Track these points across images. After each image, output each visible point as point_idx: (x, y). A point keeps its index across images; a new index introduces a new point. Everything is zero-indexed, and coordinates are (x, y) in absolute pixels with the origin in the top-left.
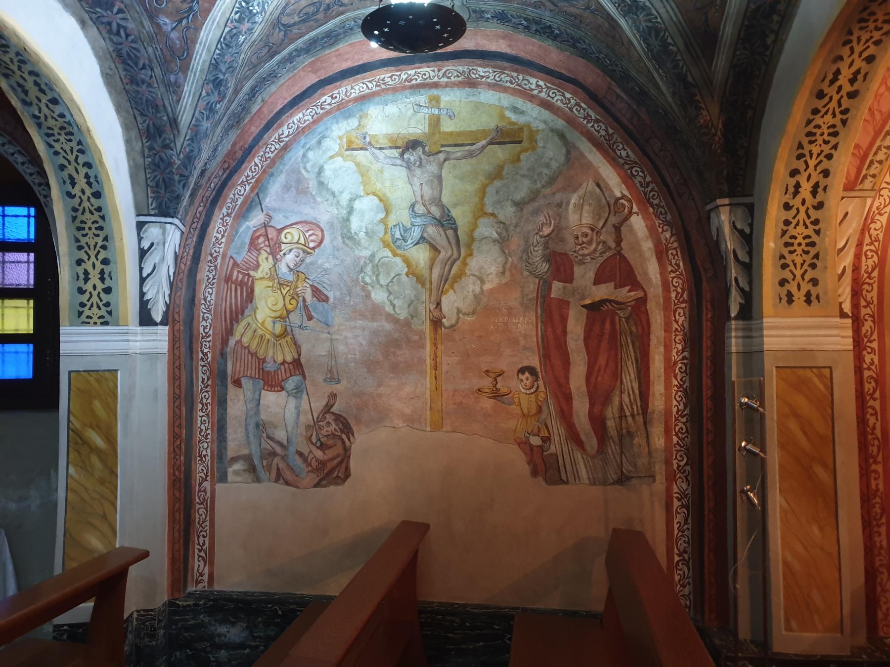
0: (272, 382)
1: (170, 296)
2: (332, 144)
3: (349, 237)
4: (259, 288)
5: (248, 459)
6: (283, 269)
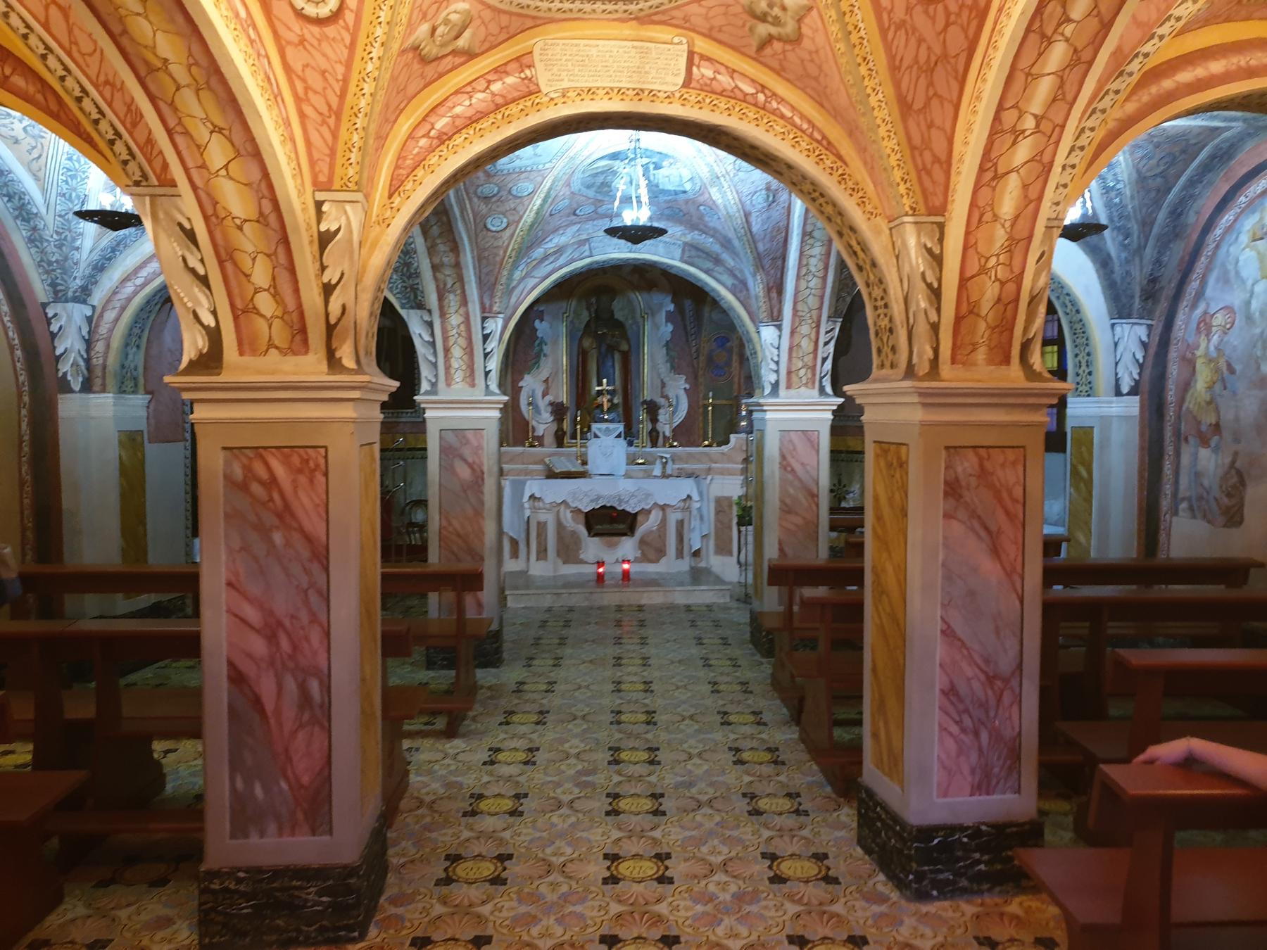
0: (1204, 441)
1: (1140, 374)
2: (1244, 238)
3: (1249, 318)
4: (1200, 365)
5: (1189, 499)
6: (1212, 348)
